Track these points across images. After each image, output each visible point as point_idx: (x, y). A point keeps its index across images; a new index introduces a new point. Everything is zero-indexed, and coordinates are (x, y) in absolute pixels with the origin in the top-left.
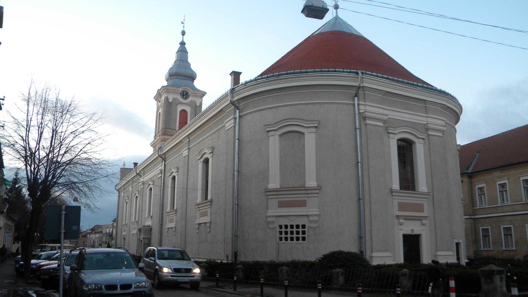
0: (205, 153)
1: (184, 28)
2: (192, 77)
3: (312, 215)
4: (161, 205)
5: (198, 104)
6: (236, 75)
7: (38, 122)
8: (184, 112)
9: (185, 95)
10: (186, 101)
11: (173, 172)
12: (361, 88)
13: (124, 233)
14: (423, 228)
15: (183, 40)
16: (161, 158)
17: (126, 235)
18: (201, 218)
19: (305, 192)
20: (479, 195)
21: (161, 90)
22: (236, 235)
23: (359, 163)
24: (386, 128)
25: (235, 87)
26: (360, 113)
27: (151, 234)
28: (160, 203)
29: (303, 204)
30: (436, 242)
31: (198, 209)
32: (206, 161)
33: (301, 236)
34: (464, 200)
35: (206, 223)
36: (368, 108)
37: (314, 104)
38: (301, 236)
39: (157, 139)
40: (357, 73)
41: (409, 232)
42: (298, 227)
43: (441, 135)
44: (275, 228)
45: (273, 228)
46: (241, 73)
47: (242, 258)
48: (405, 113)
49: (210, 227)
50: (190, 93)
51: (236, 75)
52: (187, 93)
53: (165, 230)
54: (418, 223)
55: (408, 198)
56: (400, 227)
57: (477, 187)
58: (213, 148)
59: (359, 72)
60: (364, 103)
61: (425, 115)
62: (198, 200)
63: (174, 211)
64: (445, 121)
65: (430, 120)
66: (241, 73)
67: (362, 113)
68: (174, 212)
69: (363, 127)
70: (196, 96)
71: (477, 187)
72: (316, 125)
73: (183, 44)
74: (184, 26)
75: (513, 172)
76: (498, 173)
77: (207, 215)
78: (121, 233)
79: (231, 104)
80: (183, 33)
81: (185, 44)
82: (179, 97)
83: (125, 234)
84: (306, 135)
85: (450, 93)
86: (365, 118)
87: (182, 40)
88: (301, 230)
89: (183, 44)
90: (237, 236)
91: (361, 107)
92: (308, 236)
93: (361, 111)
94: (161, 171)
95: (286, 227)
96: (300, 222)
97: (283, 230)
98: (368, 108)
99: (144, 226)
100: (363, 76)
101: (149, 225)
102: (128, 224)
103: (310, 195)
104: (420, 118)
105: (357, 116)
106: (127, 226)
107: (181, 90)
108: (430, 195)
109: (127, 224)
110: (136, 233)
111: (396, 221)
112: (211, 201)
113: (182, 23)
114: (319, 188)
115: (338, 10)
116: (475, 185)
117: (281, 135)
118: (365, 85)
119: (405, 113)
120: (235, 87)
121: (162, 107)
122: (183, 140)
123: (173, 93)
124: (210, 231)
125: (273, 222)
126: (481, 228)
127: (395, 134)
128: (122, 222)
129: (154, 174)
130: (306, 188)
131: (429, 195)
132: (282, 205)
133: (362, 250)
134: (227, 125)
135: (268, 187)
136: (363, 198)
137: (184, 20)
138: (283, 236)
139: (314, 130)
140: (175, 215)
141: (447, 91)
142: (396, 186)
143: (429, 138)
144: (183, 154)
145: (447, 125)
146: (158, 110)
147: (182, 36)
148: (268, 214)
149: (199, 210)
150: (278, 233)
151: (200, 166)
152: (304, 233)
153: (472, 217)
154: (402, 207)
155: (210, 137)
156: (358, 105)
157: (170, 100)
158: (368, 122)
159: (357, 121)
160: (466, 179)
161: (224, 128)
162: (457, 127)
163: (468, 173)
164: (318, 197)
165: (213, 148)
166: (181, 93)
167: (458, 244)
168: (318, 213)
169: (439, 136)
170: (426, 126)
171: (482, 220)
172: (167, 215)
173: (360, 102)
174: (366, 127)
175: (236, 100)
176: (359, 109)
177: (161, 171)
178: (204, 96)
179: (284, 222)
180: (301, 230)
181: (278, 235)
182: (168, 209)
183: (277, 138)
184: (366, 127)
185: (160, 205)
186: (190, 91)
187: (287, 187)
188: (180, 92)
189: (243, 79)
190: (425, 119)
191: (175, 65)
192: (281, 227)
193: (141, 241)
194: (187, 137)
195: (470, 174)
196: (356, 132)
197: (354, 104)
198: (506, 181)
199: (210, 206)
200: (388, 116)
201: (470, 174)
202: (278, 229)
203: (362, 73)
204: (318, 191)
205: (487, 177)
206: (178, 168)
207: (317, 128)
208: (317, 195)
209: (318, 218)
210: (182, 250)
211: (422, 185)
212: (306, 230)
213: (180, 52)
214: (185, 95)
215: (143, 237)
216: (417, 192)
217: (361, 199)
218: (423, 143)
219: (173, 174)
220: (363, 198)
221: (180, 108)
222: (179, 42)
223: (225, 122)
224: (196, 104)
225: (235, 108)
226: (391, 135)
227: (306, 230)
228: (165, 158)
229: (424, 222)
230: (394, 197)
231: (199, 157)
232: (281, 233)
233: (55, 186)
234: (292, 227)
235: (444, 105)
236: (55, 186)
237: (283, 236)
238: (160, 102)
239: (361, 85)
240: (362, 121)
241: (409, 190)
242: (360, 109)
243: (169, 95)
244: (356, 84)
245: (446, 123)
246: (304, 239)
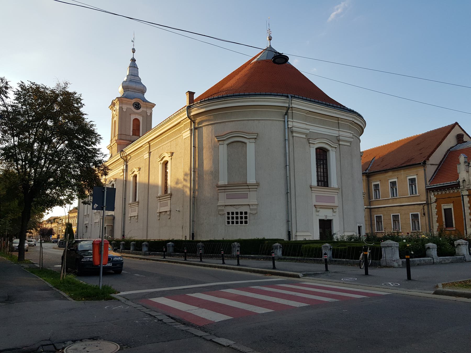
0: (164, 157)
2: (143, 90)
3: (252, 205)
4: (124, 198)
5: (149, 114)
6: (191, 94)
8: (136, 121)
9: (137, 106)
10: (138, 111)
11: (134, 171)
12: (290, 108)
13: (87, 222)
14: (334, 214)
15: (133, 58)
16: (122, 160)
17: (88, 224)
18: (161, 208)
19: (247, 187)
20: (374, 190)
21: (116, 100)
22: (193, 222)
23: (288, 166)
24: (308, 140)
25: (191, 105)
26: (288, 128)
27: (114, 223)
28: (123, 197)
29: (246, 196)
30: (344, 225)
31: (159, 201)
32: (166, 163)
33: (244, 220)
34: (365, 194)
35: (166, 212)
36: (295, 124)
37: (254, 120)
38: (244, 220)
39: (114, 143)
40: (288, 97)
41: (323, 218)
42: (241, 213)
43: (349, 144)
44: (225, 214)
45: (223, 215)
46: (195, 93)
47: (198, 238)
48: (321, 127)
49: (170, 214)
50: (141, 104)
51: (191, 94)
52: (139, 104)
53: (127, 219)
55: (323, 192)
56: (317, 214)
57: (373, 184)
58: (172, 154)
59: (289, 96)
60: (292, 120)
61: (338, 130)
62: (159, 194)
63: (136, 203)
64: (352, 133)
65: (341, 133)
66: (195, 93)
67: (290, 128)
68: (137, 204)
69: (291, 138)
70: (147, 108)
71: (373, 184)
72: (256, 137)
73: (133, 60)
75: (402, 173)
76: (390, 174)
77: (136, 211)
78: (83, 222)
79: (188, 118)
80: (134, 51)
81: (135, 61)
82: (132, 108)
83: (135, 214)
84: (248, 144)
85: (357, 112)
86: (292, 132)
87: (132, 57)
88: (244, 215)
89: (133, 60)
90: (194, 221)
91: (289, 123)
92: (249, 220)
93: (290, 126)
94: (123, 170)
95: (233, 213)
96: (243, 209)
97: (230, 216)
98: (295, 124)
99: (108, 216)
100: (292, 99)
101: (112, 214)
102: (90, 214)
103: (250, 190)
105: (286, 130)
106: (89, 216)
107: (133, 101)
108: (340, 190)
109: (89, 215)
110: (99, 222)
111: (314, 209)
112: (171, 194)
113: (132, 41)
114: (257, 185)
115: (271, 41)
116: (372, 182)
117: (228, 145)
118: (293, 106)
119: (321, 127)
120: (191, 105)
121: (117, 115)
122: (144, 145)
123: (126, 104)
124: (170, 218)
125: (223, 210)
126: (375, 216)
127: (314, 144)
128: (84, 213)
129: (116, 173)
130: (248, 184)
131: (339, 190)
132: (228, 197)
133: (290, 230)
134: (184, 135)
135: (218, 184)
136: (290, 192)
137: (134, 39)
138: (230, 220)
139: (254, 140)
140: (137, 205)
141: (355, 110)
143: (340, 146)
144: (144, 157)
145: (354, 137)
146: (113, 118)
147: (133, 53)
148: (219, 204)
149: (160, 202)
150: (226, 218)
151: (160, 167)
152: (246, 218)
153: (369, 207)
154: (318, 198)
155: (169, 144)
156: (288, 121)
158: (294, 134)
159: (287, 134)
160: (365, 178)
161: (181, 137)
162: (361, 138)
163: (367, 173)
164: (256, 191)
165: (172, 154)
167: (359, 227)
168: (257, 203)
169: (348, 146)
170: (338, 138)
171: (376, 210)
172: (130, 206)
173: (289, 120)
174: (293, 139)
175: (192, 115)
176: (288, 125)
177: (123, 170)
178: (154, 107)
179: (231, 210)
180: (244, 215)
181: (227, 220)
182: (131, 201)
183: (225, 146)
184: (293, 139)
185: (123, 198)
186: (142, 103)
187: (233, 183)
188: (133, 103)
189: (195, 97)
190: (337, 132)
191: (127, 79)
192: (228, 213)
193: (105, 228)
194: (147, 143)
195: (368, 174)
196: (286, 142)
197: (284, 121)
198: (396, 180)
199: (170, 198)
200: (310, 131)
201: (368, 174)
202: (226, 216)
203: (292, 97)
204: (256, 187)
205: (381, 176)
206: (140, 169)
207: (256, 139)
208: (256, 190)
209: (257, 206)
211: (334, 181)
212: (248, 215)
213: (131, 68)
214: (137, 106)
215: (107, 225)
216: (329, 188)
217: (289, 193)
218: (335, 151)
219: (135, 173)
220: (290, 192)
221: (133, 117)
222: (130, 59)
223: (182, 132)
224: (147, 114)
225: (191, 122)
226: (311, 145)
227: (248, 215)
228: (127, 159)
230: (313, 192)
231: (160, 160)
232: (228, 218)
234: (237, 213)
235: (352, 121)
237: (230, 220)
238: (114, 111)
239: (291, 106)
240: (290, 133)
242: (288, 125)
243: (123, 105)
244: (287, 105)
245: (353, 135)
246: (246, 222)
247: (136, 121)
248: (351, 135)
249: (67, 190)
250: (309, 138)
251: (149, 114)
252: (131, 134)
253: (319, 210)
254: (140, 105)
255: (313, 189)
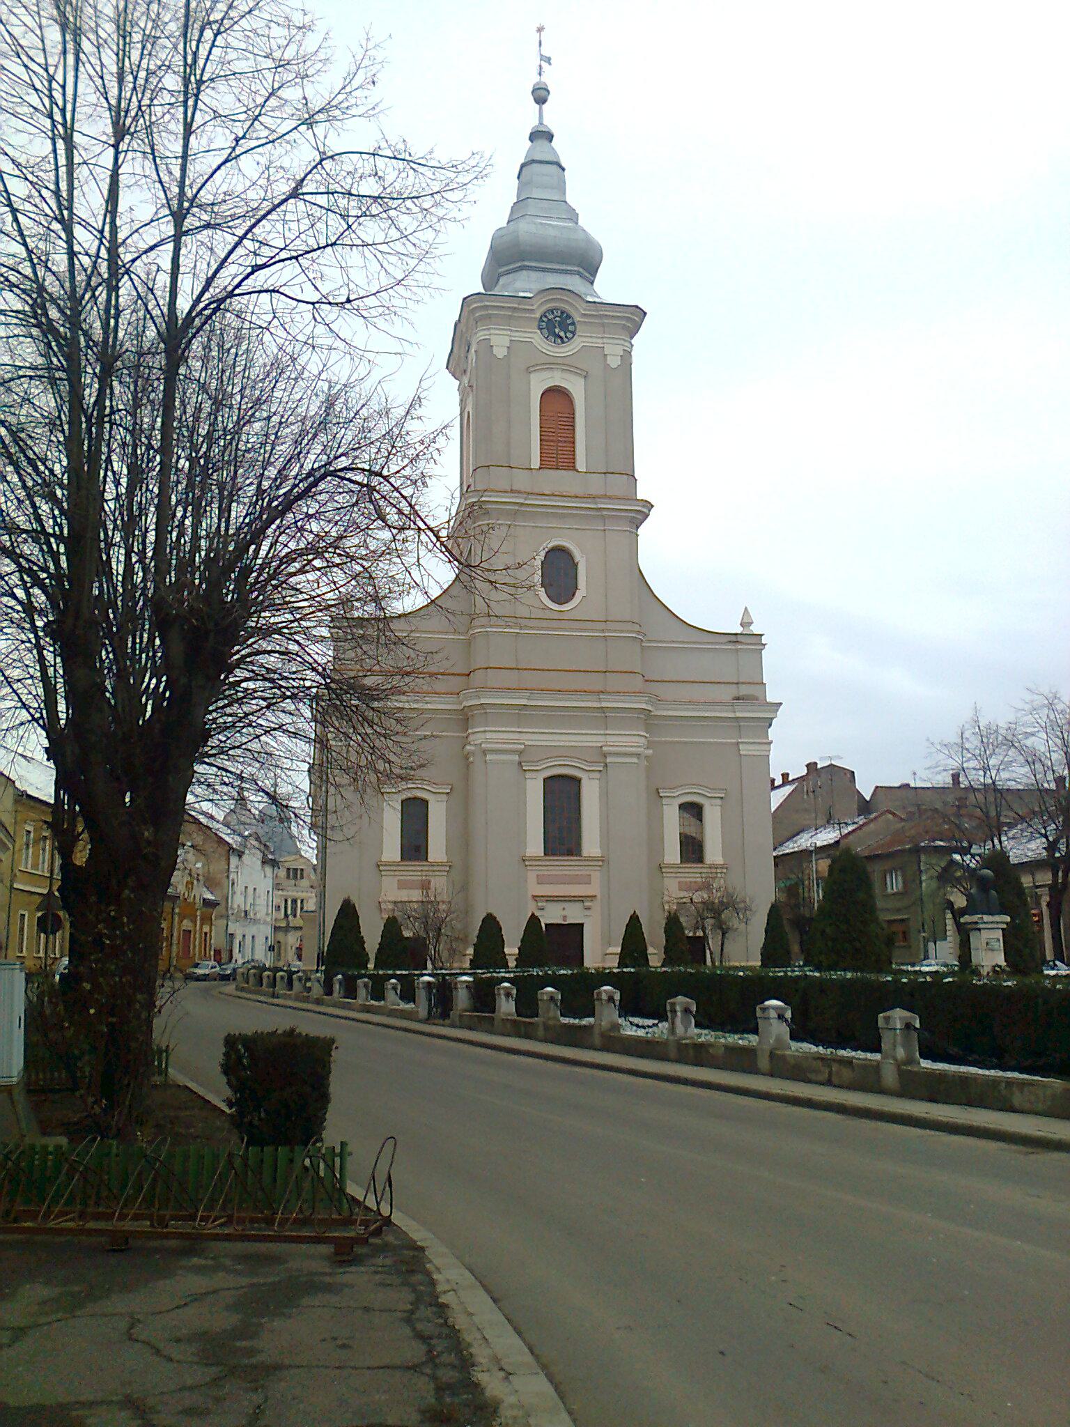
1: (540, 74)
5: (614, 362)
7: (114, 1251)
8: (556, 397)
14: (587, 913)
15: (541, 123)
50: (577, 318)
52: (569, 317)
54: (579, 905)
55: (563, 866)
74: (540, 74)
80: (540, 96)
87: (537, 123)
89: (541, 135)
104: (590, 738)
142: (535, 846)
147: (537, 106)
157: (500, 352)
166: (541, 320)
188: (538, 315)
210: (632, 1016)
211: (591, 844)
221: (539, 384)
229: (587, 904)
233: (25, 577)
236: (25, 577)
241: (572, 855)
247: (556, 397)
248: (643, 740)
249: (79, 1064)
250: (523, 760)
251: (614, 362)
252: (536, 464)
253: (544, 904)
254: (573, 324)
255: (381, 868)
